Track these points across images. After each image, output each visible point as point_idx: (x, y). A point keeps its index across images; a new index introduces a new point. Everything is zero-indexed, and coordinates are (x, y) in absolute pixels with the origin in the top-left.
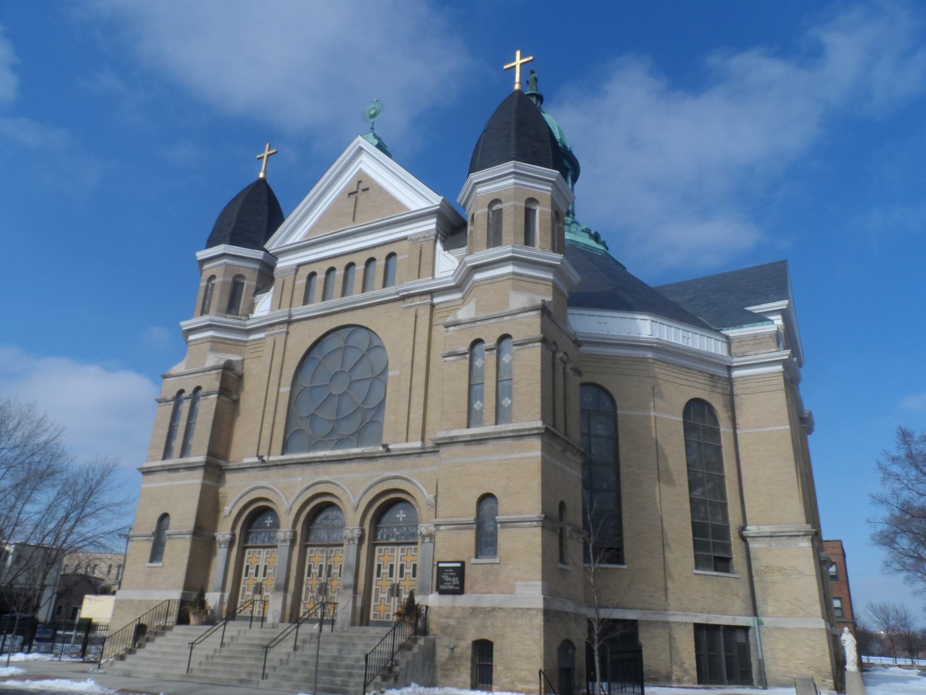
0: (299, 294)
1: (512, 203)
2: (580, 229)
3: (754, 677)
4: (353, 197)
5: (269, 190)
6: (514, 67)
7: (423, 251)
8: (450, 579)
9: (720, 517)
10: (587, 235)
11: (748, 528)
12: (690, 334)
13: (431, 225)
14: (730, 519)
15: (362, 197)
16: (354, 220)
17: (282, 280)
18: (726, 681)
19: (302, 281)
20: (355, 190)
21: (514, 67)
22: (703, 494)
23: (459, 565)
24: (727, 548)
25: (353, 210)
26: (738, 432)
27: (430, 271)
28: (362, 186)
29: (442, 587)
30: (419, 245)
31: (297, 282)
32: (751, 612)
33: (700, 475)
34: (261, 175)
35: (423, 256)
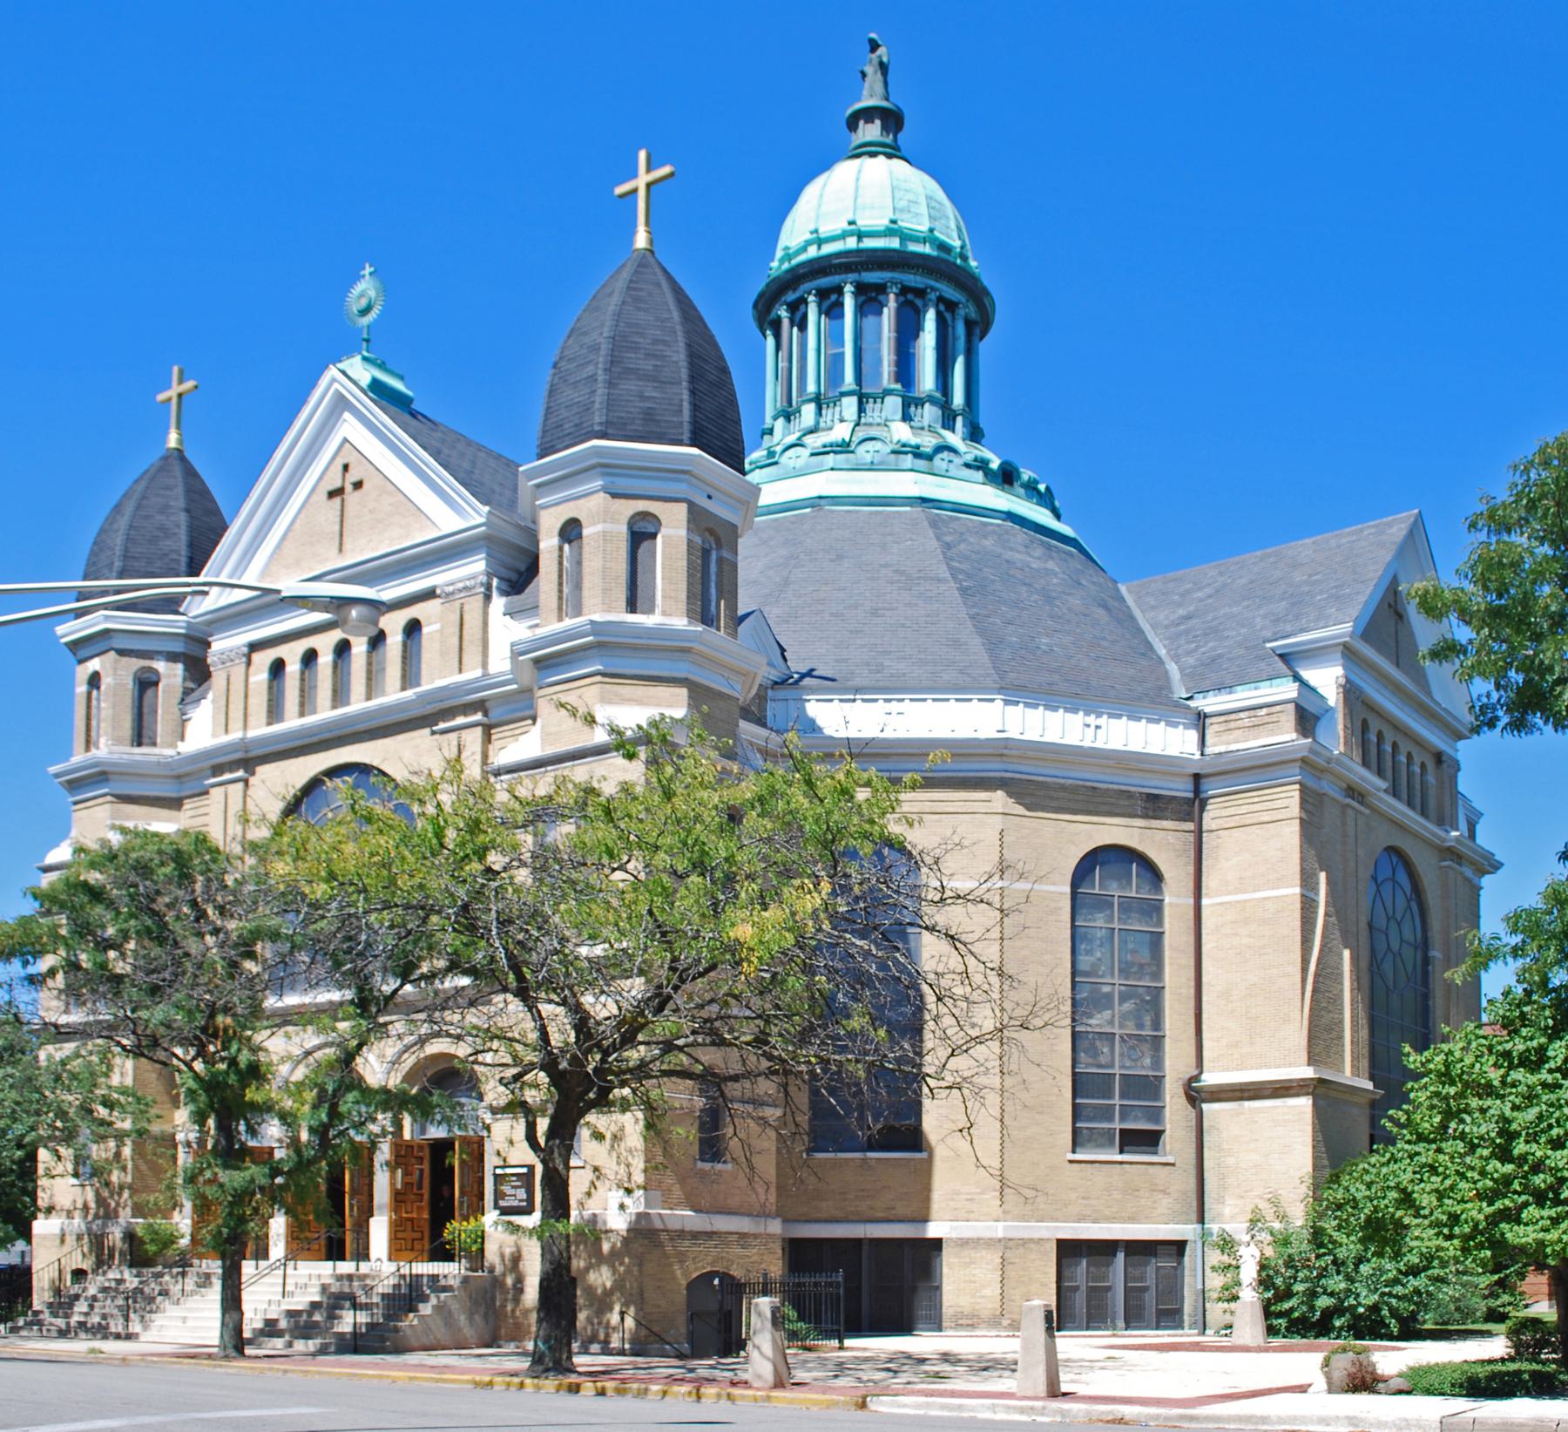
0: (259, 702)
1: (599, 527)
2: (961, 461)
3: (1186, 1317)
4: (337, 500)
5: (190, 473)
6: (635, 191)
7: (466, 617)
8: (513, 1192)
9: (1147, 1061)
10: (979, 475)
11: (1204, 1077)
12: (1103, 720)
13: (476, 566)
14: (1167, 1063)
15: (352, 497)
16: (341, 550)
17: (224, 677)
18: (1121, 1323)
19: (260, 676)
20: (338, 484)
21: (635, 191)
22: (320, 1169)
23: (524, 1170)
24: (1156, 1114)
25: (337, 527)
26: (1205, 901)
27: (479, 658)
28: (353, 476)
29: (502, 1203)
30: (457, 604)
31: (252, 680)
32: (1194, 1216)
33: (1106, 989)
34: (173, 440)
35: (466, 627)
